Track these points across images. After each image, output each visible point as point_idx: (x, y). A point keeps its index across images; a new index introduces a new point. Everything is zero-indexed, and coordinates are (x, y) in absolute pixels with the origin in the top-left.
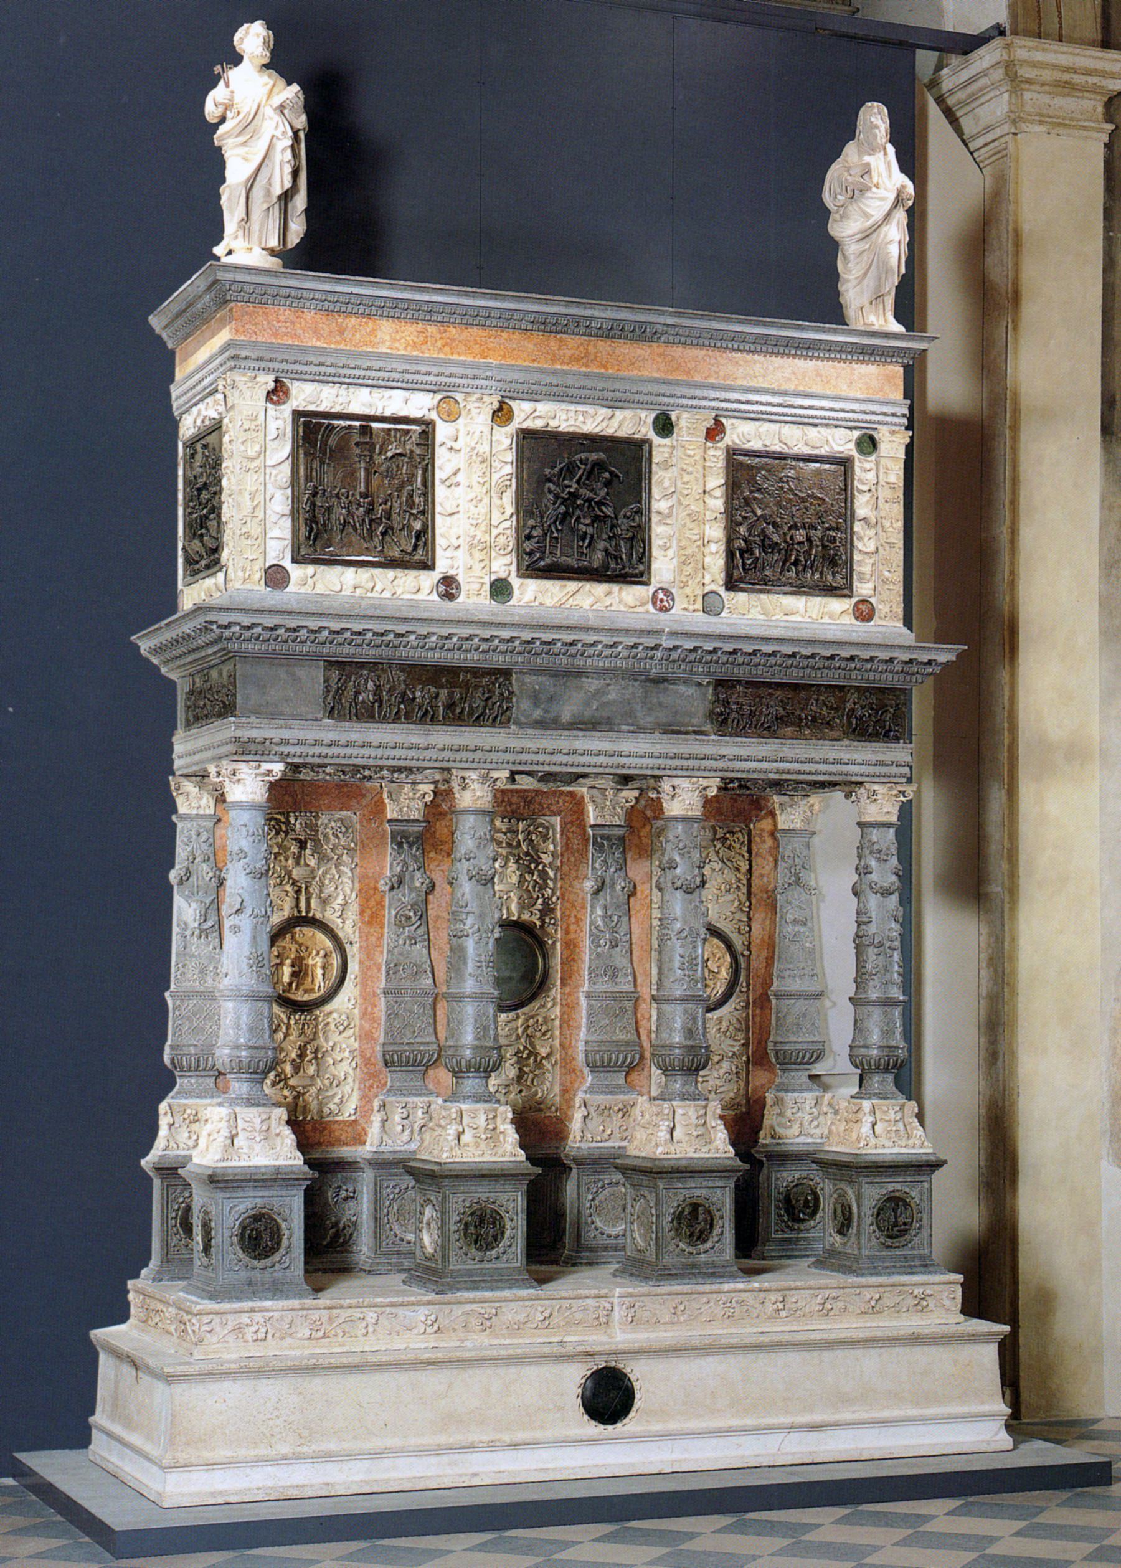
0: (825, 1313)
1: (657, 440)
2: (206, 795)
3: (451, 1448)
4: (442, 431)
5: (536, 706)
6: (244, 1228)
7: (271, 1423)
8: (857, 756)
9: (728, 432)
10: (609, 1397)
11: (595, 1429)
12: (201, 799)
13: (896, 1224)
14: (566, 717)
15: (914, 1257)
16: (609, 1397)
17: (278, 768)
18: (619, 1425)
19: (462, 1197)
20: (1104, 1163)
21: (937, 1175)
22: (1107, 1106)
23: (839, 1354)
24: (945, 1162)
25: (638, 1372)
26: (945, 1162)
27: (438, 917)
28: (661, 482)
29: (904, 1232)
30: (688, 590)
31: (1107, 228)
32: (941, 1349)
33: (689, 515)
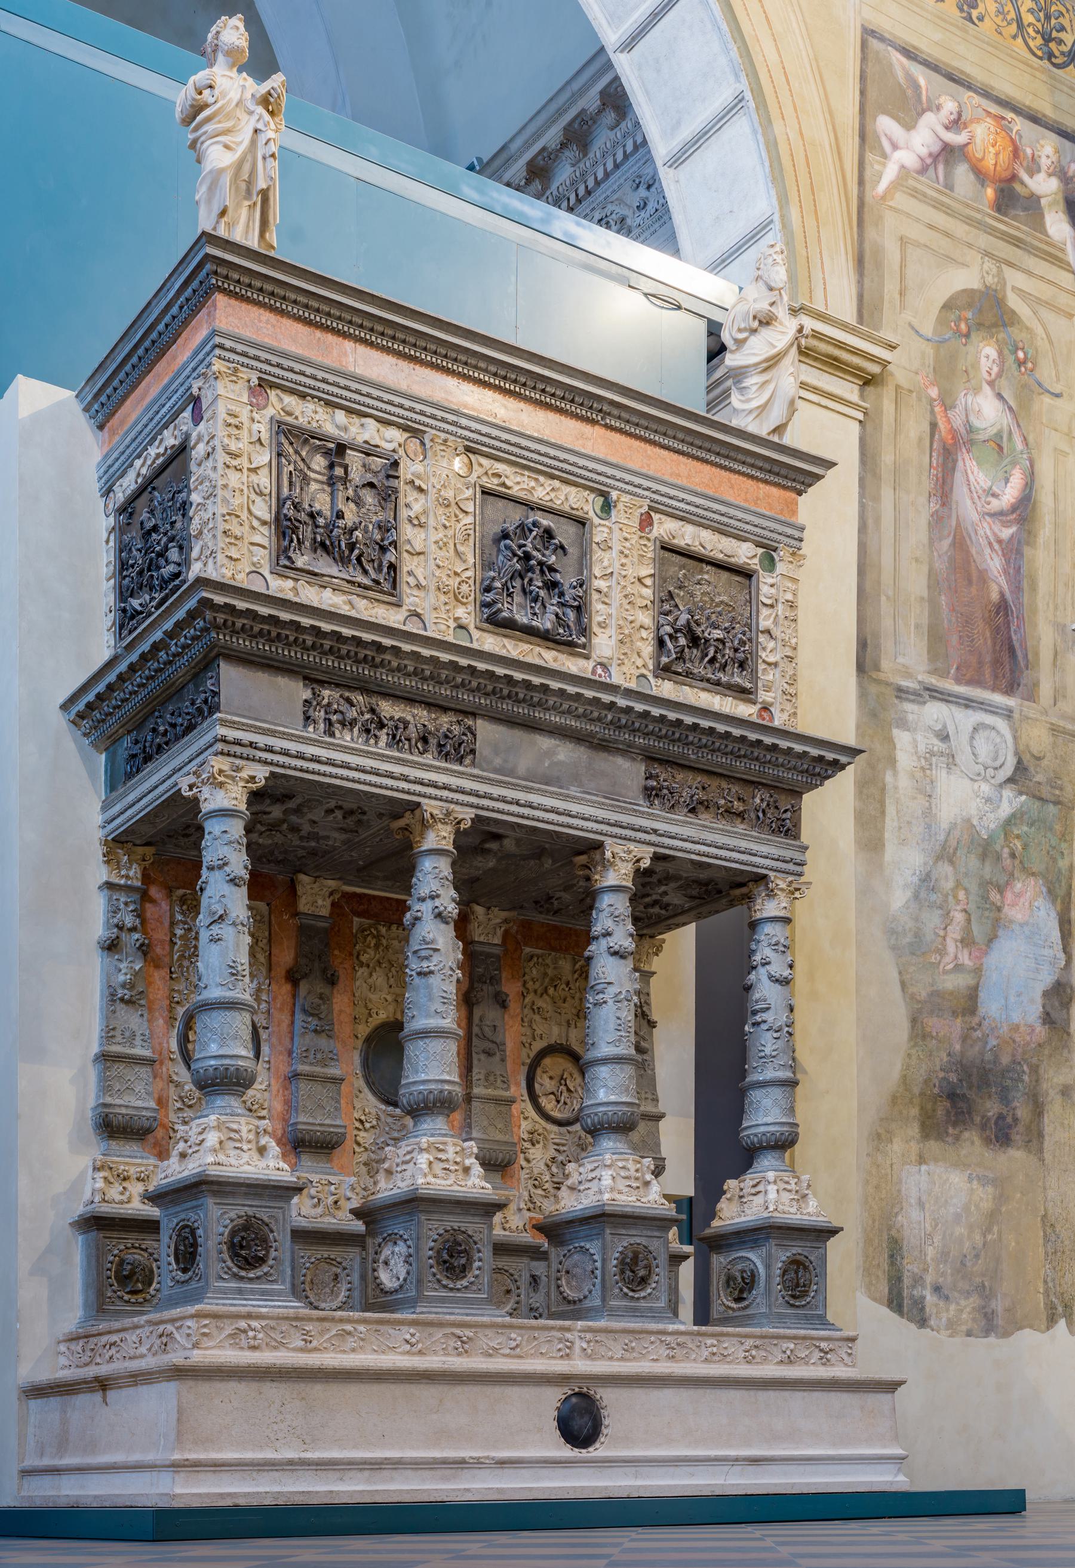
0: (749, 1360)
1: (596, 521)
2: (135, 866)
3: (445, 1462)
4: (409, 469)
5: (497, 753)
6: (233, 1233)
7: (275, 1427)
8: (764, 849)
9: (656, 525)
10: (580, 1423)
11: (568, 1452)
12: (130, 868)
13: (797, 1285)
14: (521, 770)
15: (813, 1316)
16: (580, 1423)
17: (261, 773)
18: (591, 1449)
19: (436, 1224)
20: (858, 1294)
21: (832, 1243)
22: (861, 1245)
23: (771, 1395)
24: (842, 1229)
25: (606, 1396)
26: (842, 1229)
27: (341, 1011)
28: (601, 561)
29: (805, 1294)
30: (625, 669)
31: (862, 495)
32: (851, 1395)
33: (626, 596)
